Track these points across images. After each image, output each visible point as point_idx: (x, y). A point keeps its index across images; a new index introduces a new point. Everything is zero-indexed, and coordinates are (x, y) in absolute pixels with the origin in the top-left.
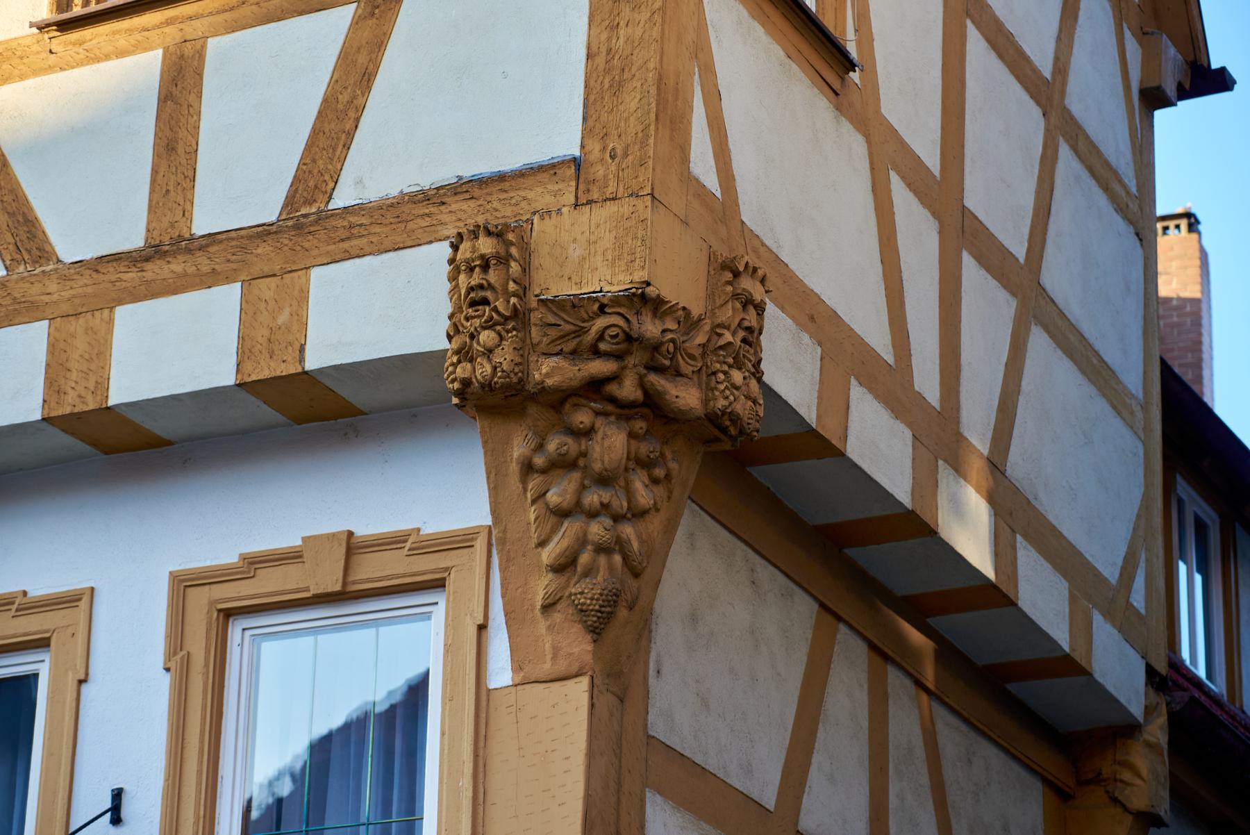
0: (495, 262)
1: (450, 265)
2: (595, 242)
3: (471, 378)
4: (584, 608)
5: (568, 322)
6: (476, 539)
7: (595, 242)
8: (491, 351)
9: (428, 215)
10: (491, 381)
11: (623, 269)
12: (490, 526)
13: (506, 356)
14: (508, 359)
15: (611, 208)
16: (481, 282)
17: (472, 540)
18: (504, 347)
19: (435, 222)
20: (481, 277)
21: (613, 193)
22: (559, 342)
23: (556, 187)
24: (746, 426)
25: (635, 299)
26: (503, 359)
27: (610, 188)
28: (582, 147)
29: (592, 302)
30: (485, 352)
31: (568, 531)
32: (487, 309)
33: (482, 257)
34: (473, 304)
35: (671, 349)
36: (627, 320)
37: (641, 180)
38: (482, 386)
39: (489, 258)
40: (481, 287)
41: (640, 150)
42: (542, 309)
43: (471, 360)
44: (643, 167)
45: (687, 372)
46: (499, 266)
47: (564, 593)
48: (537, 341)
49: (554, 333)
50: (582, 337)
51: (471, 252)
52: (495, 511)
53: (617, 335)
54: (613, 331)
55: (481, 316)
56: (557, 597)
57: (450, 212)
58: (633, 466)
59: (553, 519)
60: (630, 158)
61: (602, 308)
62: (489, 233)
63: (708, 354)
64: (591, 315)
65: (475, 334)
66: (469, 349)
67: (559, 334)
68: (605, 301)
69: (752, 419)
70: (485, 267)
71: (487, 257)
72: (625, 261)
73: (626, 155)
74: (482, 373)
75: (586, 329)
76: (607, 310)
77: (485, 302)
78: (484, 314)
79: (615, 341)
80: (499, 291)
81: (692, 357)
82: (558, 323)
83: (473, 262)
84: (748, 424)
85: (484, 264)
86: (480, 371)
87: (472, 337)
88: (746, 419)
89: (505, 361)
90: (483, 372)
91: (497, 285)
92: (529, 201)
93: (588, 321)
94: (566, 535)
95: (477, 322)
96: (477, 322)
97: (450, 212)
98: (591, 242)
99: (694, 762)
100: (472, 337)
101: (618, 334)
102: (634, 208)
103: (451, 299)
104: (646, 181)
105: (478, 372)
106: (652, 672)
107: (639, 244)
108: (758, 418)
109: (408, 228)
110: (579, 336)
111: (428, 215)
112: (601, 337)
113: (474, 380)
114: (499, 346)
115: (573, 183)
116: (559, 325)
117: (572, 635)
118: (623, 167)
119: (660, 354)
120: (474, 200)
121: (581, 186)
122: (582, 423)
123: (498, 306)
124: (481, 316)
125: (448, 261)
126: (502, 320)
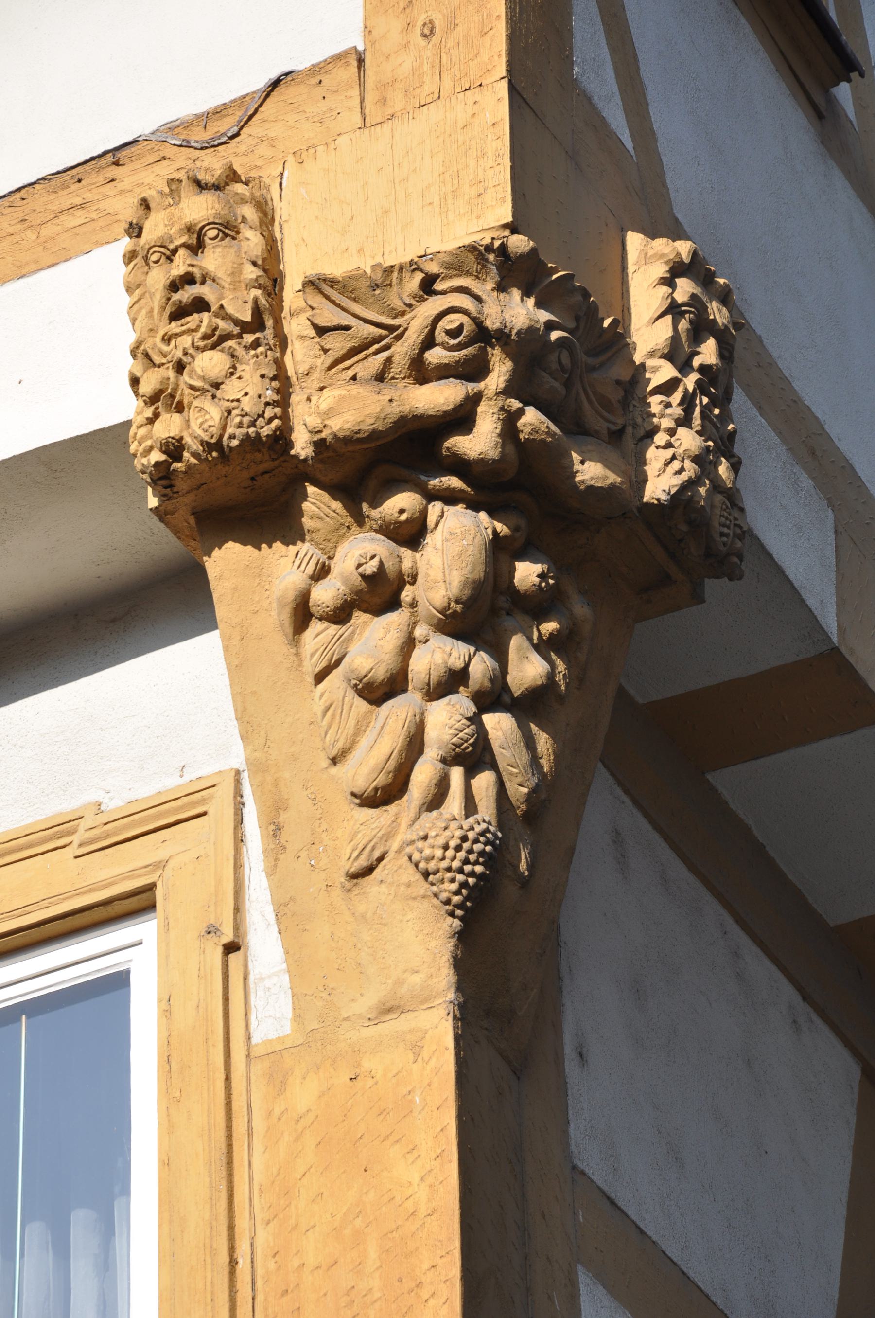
0: (215, 232)
1: (127, 264)
2: (405, 180)
3: (182, 438)
4: (432, 866)
5: (366, 321)
6: (211, 797)
7: (405, 180)
8: (217, 385)
9: (81, 206)
10: (221, 436)
11: (462, 211)
12: (238, 773)
13: (247, 390)
14: (251, 394)
15: (433, 113)
16: (190, 269)
17: (203, 801)
18: (242, 373)
19: (94, 215)
20: (188, 262)
21: (433, 93)
22: (347, 363)
23: (323, 106)
24: (717, 538)
25: (491, 257)
26: (243, 393)
27: (426, 88)
28: (368, 31)
29: (408, 274)
30: (207, 387)
31: (390, 721)
32: (205, 316)
33: (189, 229)
34: (179, 313)
35: (566, 360)
36: (478, 299)
37: (486, 60)
38: (208, 446)
39: (204, 226)
40: (188, 279)
41: (478, 11)
42: (317, 300)
43: (180, 408)
44: (487, 38)
45: (597, 428)
46: (222, 240)
47: (390, 847)
48: (307, 367)
49: (338, 344)
50: (392, 349)
51: (166, 225)
52: (245, 710)
53: (460, 329)
54: (452, 321)
55: (193, 331)
56: (377, 854)
57: (121, 192)
58: (506, 606)
59: (361, 705)
60: (459, 29)
61: (428, 286)
62: (200, 186)
63: (634, 406)
64: (408, 302)
65: (185, 359)
66: (175, 389)
67: (349, 345)
68: (433, 268)
69: (727, 535)
70: (197, 247)
71: (198, 228)
72: (467, 197)
73: (453, 25)
74: (201, 424)
75: (401, 329)
76: (439, 286)
77: (200, 305)
78: (199, 326)
79: (456, 342)
80: (227, 286)
81: (606, 404)
82: (345, 323)
83: (171, 242)
84: (722, 534)
85: (194, 241)
86: (200, 420)
87: (180, 367)
88: (716, 524)
89: (247, 398)
90: (206, 421)
91: (220, 274)
92: (272, 143)
93: (403, 314)
94: (386, 730)
95: (186, 341)
96: (186, 341)
97: (121, 192)
98: (397, 181)
99: (664, 1253)
100: (180, 367)
101: (461, 326)
102: (476, 106)
103: (134, 321)
104: (496, 58)
105: (195, 426)
106: (569, 1050)
107: (491, 163)
108: (738, 531)
109: (42, 235)
110: (387, 347)
111: (81, 206)
112: (429, 342)
113: (188, 440)
114: (232, 374)
115: (356, 92)
116: (347, 328)
117: (410, 923)
118: (448, 46)
119: (544, 370)
120: (165, 163)
121: (370, 98)
122: (402, 511)
123: (225, 306)
124: (193, 331)
125: (124, 256)
126: (236, 330)
